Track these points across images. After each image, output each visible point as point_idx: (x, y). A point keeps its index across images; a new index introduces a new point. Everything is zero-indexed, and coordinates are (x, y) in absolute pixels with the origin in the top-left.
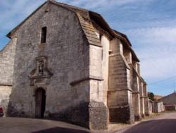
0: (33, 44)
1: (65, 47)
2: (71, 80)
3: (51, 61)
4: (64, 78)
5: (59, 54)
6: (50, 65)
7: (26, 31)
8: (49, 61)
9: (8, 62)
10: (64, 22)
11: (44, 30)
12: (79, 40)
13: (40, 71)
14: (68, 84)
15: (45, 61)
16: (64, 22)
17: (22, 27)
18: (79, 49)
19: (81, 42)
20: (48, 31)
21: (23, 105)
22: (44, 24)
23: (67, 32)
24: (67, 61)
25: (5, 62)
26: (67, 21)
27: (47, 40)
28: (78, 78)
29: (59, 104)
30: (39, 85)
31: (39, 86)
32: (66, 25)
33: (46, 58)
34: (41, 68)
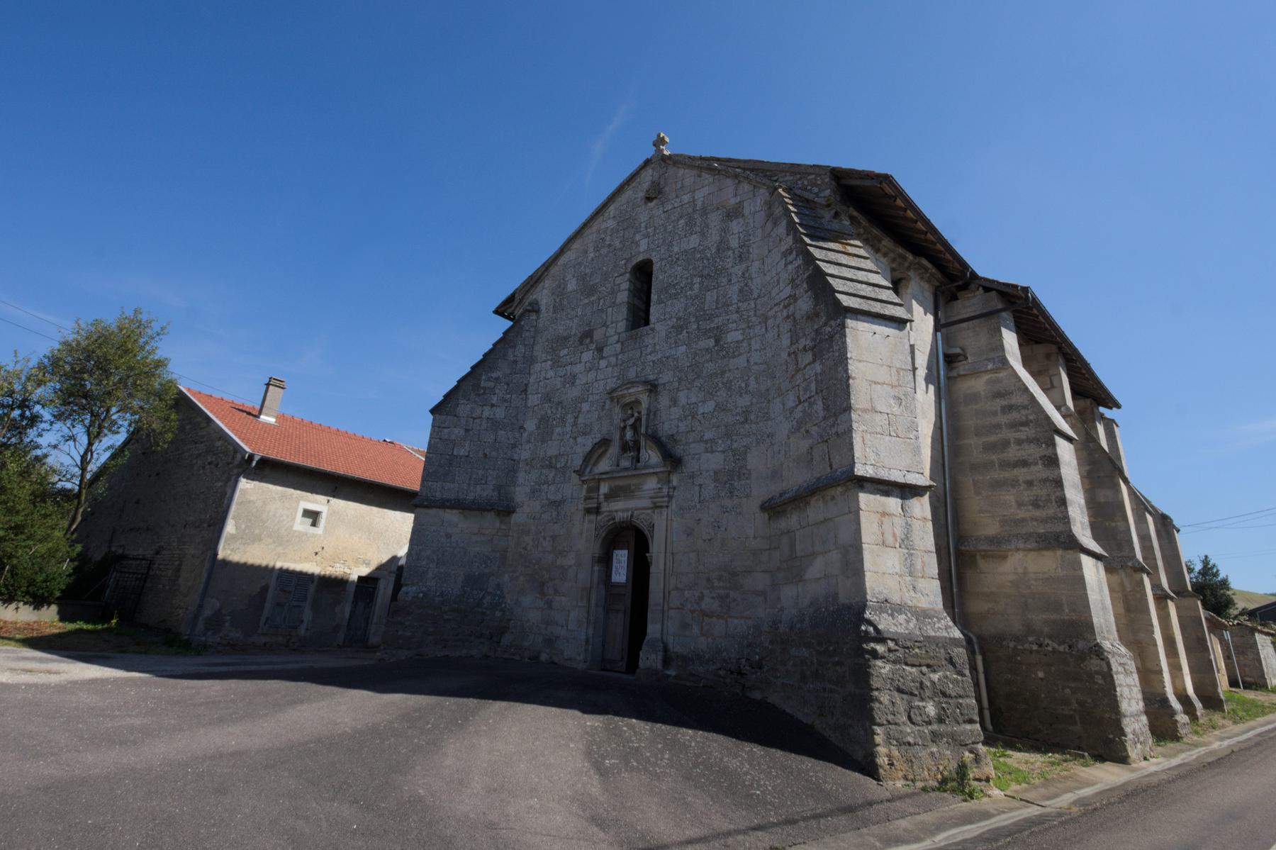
0: (598, 335)
1: (733, 336)
2: (762, 491)
3: (674, 402)
4: (732, 477)
5: (710, 367)
6: (670, 421)
7: (572, 285)
8: (664, 401)
9: (500, 413)
10: (725, 230)
11: (643, 272)
12: (793, 298)
13: (625, 447)
14: (752, 506)
15: (644, 399)
16: (725, 230)
17: (555, 270)
18: (794, 339)
19: (805, 304)
20: (658, 278)
21: (549, 604)
22: (642, 249)
23: (738, 270)
24: (744, 401)
25: (487, 412)
26: (735, 226)
27: (654, 311)
28: (797, 478)
29: (709, 604)
30: (620, 509)
31: (620, 516)
32: (734, 243)
33: (653, 388)
34: (629, 435)
